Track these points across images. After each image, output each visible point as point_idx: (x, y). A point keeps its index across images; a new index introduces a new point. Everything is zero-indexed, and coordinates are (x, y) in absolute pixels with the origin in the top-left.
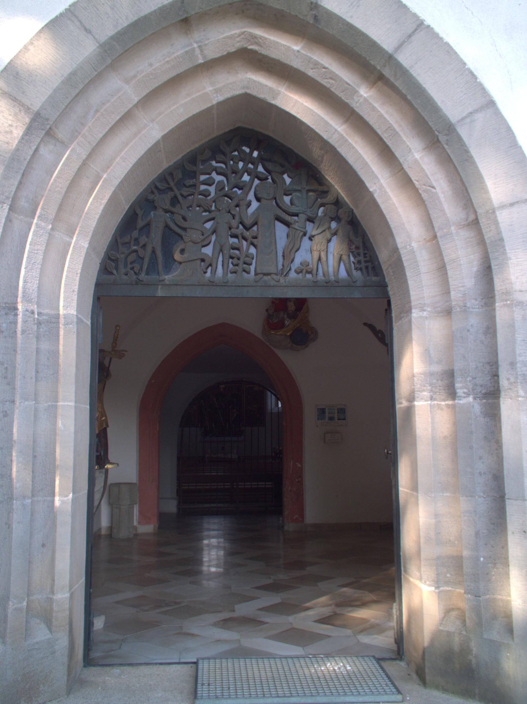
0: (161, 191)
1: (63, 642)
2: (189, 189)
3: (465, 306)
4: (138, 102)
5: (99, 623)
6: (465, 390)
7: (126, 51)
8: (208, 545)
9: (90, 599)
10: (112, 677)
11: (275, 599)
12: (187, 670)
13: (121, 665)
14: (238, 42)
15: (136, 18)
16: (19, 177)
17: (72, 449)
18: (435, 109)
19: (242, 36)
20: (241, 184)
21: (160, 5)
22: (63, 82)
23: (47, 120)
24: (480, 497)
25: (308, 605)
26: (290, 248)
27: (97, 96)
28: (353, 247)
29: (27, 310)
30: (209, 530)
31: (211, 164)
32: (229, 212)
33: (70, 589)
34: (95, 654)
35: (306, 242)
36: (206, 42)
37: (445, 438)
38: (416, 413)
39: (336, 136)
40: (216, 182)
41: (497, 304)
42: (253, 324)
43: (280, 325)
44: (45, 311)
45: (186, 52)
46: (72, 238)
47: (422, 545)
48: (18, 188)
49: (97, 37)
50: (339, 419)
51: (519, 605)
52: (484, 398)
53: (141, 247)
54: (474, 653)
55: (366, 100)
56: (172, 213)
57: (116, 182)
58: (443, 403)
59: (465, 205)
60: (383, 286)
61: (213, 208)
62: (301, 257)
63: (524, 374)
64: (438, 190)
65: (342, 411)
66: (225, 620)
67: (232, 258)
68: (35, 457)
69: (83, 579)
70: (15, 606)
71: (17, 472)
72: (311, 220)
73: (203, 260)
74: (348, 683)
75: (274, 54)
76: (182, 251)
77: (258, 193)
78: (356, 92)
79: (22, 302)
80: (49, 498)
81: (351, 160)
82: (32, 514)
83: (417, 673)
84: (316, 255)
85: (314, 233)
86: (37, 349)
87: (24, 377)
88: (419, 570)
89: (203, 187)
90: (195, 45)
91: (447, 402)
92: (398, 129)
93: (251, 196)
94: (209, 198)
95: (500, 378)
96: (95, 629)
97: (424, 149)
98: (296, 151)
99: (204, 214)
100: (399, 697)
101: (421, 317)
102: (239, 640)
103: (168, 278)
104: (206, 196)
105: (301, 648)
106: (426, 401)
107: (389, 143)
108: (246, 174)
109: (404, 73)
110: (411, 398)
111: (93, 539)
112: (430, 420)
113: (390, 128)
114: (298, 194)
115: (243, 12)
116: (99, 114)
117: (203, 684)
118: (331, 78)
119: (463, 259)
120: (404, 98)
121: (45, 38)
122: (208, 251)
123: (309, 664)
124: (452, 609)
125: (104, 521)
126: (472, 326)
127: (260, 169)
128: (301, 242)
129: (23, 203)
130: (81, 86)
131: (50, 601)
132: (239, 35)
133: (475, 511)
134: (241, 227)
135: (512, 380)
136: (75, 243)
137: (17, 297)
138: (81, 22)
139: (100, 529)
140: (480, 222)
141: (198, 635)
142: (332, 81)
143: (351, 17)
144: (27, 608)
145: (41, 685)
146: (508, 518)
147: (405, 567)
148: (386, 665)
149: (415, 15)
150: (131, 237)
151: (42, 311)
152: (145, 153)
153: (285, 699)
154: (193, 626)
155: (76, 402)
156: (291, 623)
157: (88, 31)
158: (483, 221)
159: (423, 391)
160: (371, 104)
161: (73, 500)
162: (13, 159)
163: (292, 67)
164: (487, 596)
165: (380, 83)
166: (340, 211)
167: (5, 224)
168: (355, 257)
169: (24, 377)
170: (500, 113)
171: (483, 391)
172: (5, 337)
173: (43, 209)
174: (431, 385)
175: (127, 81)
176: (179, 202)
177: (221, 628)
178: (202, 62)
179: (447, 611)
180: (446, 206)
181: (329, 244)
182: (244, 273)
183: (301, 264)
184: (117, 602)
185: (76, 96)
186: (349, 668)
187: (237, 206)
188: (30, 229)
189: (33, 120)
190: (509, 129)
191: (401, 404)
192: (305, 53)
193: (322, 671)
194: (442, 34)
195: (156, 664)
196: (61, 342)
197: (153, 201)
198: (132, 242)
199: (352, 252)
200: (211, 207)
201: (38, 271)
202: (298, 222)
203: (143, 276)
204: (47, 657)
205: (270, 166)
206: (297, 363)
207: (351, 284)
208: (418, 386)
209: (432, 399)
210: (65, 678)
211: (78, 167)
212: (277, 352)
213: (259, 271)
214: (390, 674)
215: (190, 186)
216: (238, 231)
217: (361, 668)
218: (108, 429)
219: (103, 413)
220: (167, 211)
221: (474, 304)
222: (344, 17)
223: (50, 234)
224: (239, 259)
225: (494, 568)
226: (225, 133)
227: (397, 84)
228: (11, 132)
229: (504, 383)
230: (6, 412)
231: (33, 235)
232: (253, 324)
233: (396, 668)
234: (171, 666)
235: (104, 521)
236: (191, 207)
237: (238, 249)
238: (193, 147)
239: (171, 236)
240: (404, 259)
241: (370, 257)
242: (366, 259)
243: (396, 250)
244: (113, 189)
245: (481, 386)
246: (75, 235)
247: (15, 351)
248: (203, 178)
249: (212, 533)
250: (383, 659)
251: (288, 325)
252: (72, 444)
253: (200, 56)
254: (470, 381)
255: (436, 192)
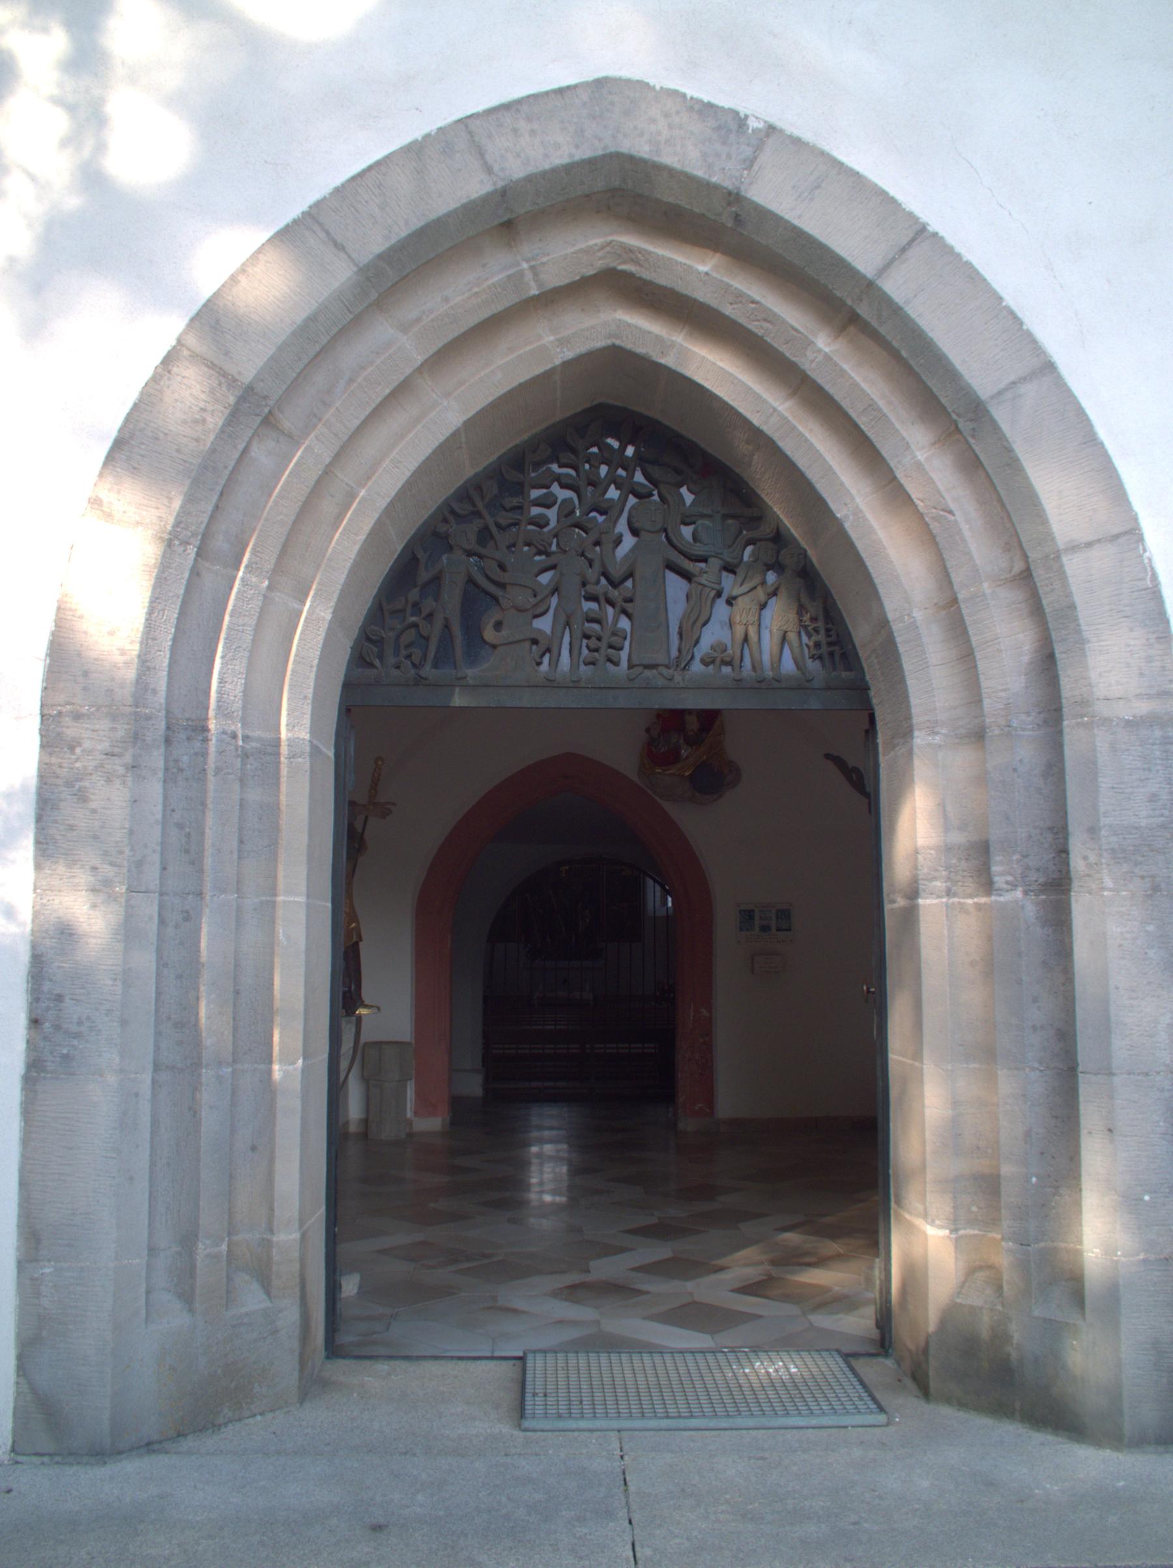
0: (460, 518)
1: (290, 1316)
2: (510, 514)
3: (1009, 726)
4: (422, 365)
5: (350, 1286)
6: (1010, 878)
7: (403, 279)
8: (539, 1155)
9: (335, 1244)
10: (376, 1377)
11: (660, 1251)
12: (506, 1370)
13: (390, 1357)
14: (600, 259)
15: (423, 223)
16: (216, 497)
17: (302, 979)
18: (951, 375)
19: (608, 249)
20: (604, 505)
21: (464, 201)
22: (294, 334)
23: (266, 397)
24: (1033, 1069)
25: (720, 1262)
26: (692, 619)
27: (351, 355)
28: (806, 617)
29: (224, 733)
30: (540, 1128)
31: (549, 470)
32: (582, 554)
33: (301, 1227)
34: (346, 1338)
35: (721, 610)
36: (545, 259)
37: (973, 964)
38: (921, 918)
39: (774, 419)
40: (559, 501)
41: (1065, 723)
42: (622, 755)
43: (672, 758)
44: (256, 733)
45: (509, 277)
46: (304, 603)
47: (928, 1157)
48: (212, 517)
49: (354, 255)
50: (778, 930)
51: (1096, 1257)
52: (1042, 892)
53: (424, 619)
54: (1015, 1341)
55: (827, 357)
56: (481, 557)
57: (382, 504)
58: (970, 901)
59: (1006, 544)
60: (860, 689)
61: (554, 548)
62: (712, 636)
63: (1112, 849)
64: (959, 517)
65: (784, 915)
66: (573, 1287)
67: (587, 637)
68: (237, 993)
69: (322, 1210)
70: (208, 1251)
71: (208, 1018)
72: (730, 569)
73: (535, 642)
74: (793, 1396)
75: (662, 279)
76: (498, 626)
77: (634, 520)
78: (811, 343)
79: (216, 718)
80: (262, 1067)
81: (802, 463)
82: (233, 1094)
83: (914, 1378)
84: (739, 631)
85: (735, 592)
86: (242, 800)
87: (219, 851)
88: (923, 1199)
89: (535, 511)
90: (525, 265)
91: (976, 900)
92: (886, 410)
93: (622, 526)
94: (545, 530)
95: (1072, 855)
96: (343, 1295)
97: (934, 444)
98: (703, 446)
99: (537, 558)
100: (882, 1418)
101: (929, 745)
102: (598, 1322)
103: (471, 673)
104: (541, 527)
105: (708, 1337)
106: (939, 897)
107: (870, 434)
108: (612, 486)
109: (895, 311)
110: (913, 894)
111: (338, 1137)
112: (945, 932)
113: (872, 406)
114: (707, 522)
115: (609, 208)
116: (355, 385)
117: (535, 1394)
118: (765, 320)
119: (1006, 642)
120: (895, 354)
121: (267, 262)
122: (544, 624)
123: (723, 1363)
124: (980, 1268)
125: (354, 1109)
126: (1021, 761)
127: (639, 477)
128: (712, 608)
129: (220, 543)
130: (324, 340)
131: (267, 1244)
132: (602, 248)
133: (1024, 1096)
134: (603, 581)
135: (1092, 858)
136: (308, 612)
137: (207, 708)
138: (327, 233)
139: (347, 1123)
140: (1034, 574)
141: (523, 1312)
142: (766, 325)
143: (800, 217)
144: (228, 1255)
145: (256, 1385)
146: (1081, 1107)
147: (897, 1196)
148: (860, 1365)
149: (911, 215)
150: (407, 600)
151: (250, 734)
152: (434, 452)
153: (681, 1420)
154: (517, 1295)
155: (308, 897)
156: (691, 1294)
157: (339, 247)
158: (1039, 574)
159: (935, 878)
160: (836, 365)
161: (303, 1071)
162: (206, 468)
163: (695, 300)
164: (1042, 1244)
165: (852, 329)
166: (782, 552)
167: (189, 580)
168: (809, 636)
169: (219, 851)
170: (1065, 385)
171: (1041, 880)
172: (187, 779)
173: (254, 552)
174: (947, 868)
175: (404, 329)
176: (492, 537)
177: (566, 1300)
178: (537, 293)
179: (971, 1272)
180: (973, 547)
181: (763, 612)
182: (608, 664)
183: (712, 647)
184: (382, 1252)
185: (316, 356)
186: (794, 1370)
187: (597, 543)
188: (231, 588)
189: (241, 399)
190: (1081, 412)
191: (893, 904)
192: (719, 277)
193: (746, 1375)
194: (959, 248)
195: (452, 1358)
196: (284, 788)
197: (446, 537)
198: (409, 610)
199: (805, 627)
200: (550, 545)
201: (245, 661)
202: (707, 573)
203: (427, 671)
204: (265, 1338)
205: (656, 472)
206: (702, 826)
207: (802, 685)
208: (925, 870)
209: (949, 893)
210: (296, 1374)
211: (315, 477)
212: (667, 806)
213: (635, 661)
214: (866, 1380)
215: (513, 509)
216: (598, 588)
217: (814, 1370)
218: (361, 944)
219: (353, 916)
220: (470, 554)
221: (1026, 722)
222: (787, 217)
223: (265, 597)
224: (599, 639)
225: (1054, 1194)
226: (576, 415)
227: (882, 331)
228: (204, 421)
229: (1077, 864)
230: (187, 912)
231: (237, 599)
232: (622, 755)
233: (877, 1370)
234: (479, 1362)
235: (354, 1109)
236: (514, 545)
237: (598, 621)
238: (517, 442)
239: (478, 599)
240: (898, 640)
241: (838, 635)
242: (829, 639)
243: (884, 624)
244: (377, 516)
245: (1038, 870)
246: (309, 599)
247: (204, 804)
248: (535, 494)
249: (547, 1133)
250: (855, 1355)
251: (687, 758)
252: (302, 971)
253: (532, 283)
254: (1018, 861)
255: (956, 521)
